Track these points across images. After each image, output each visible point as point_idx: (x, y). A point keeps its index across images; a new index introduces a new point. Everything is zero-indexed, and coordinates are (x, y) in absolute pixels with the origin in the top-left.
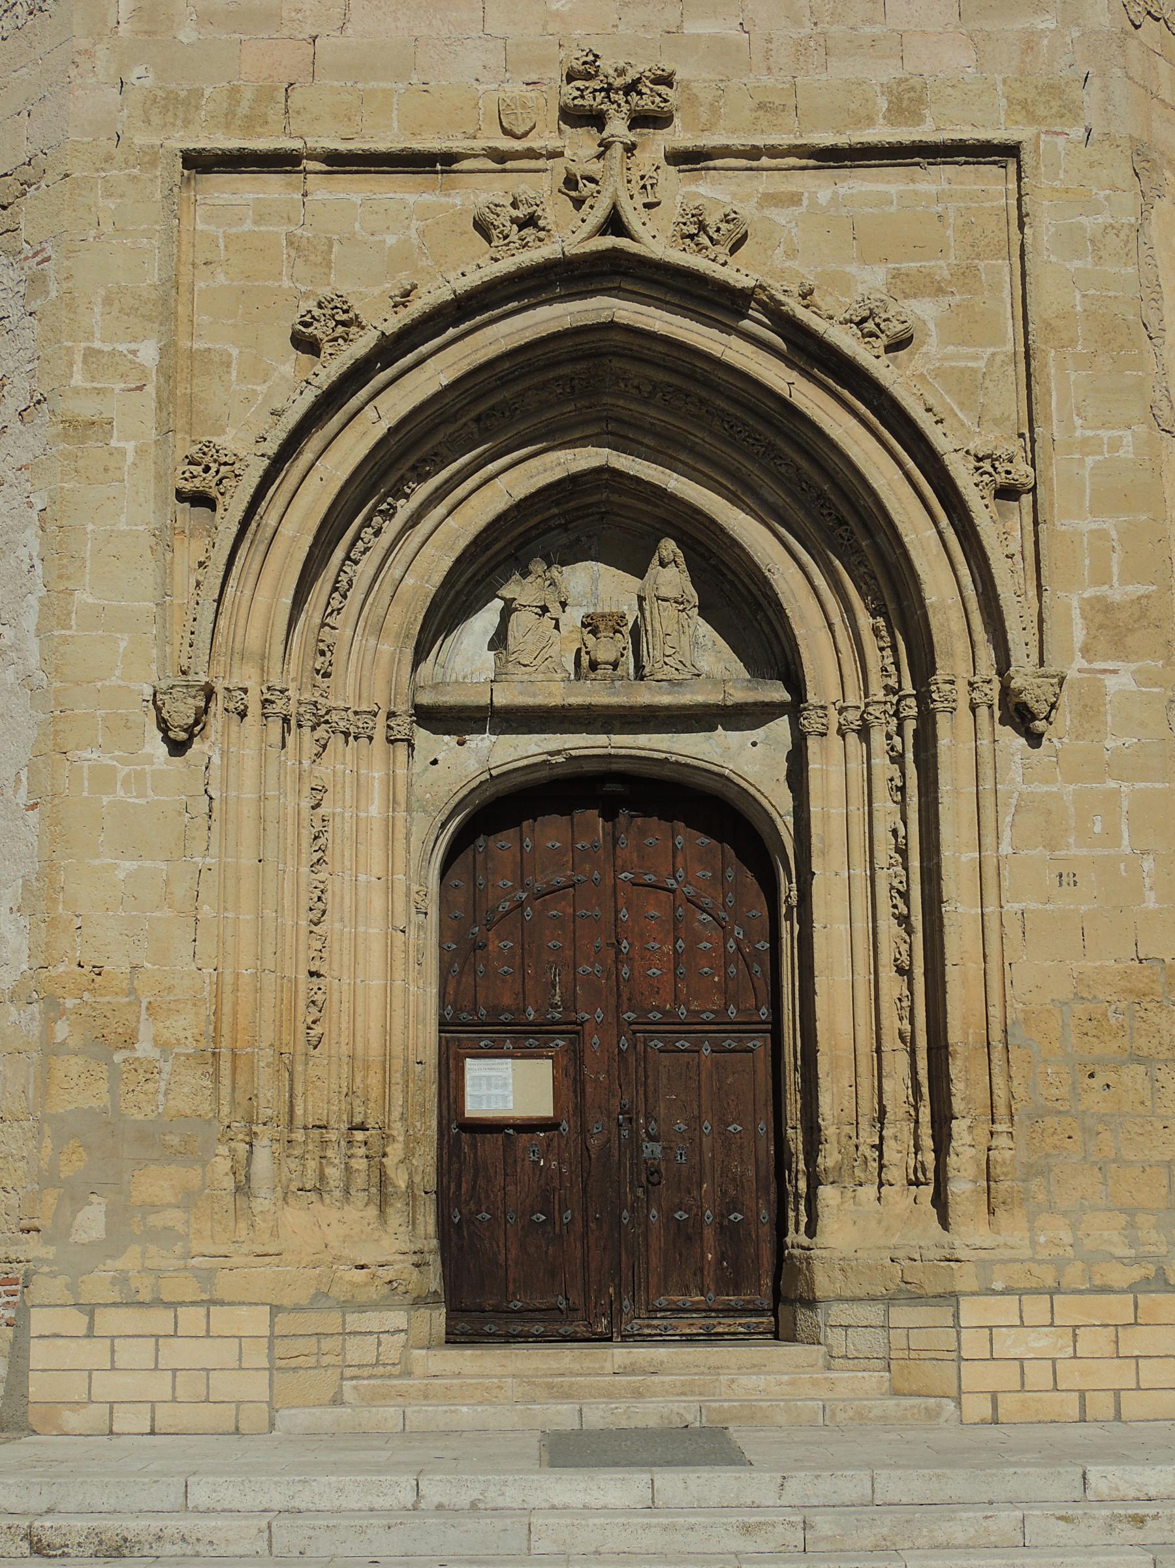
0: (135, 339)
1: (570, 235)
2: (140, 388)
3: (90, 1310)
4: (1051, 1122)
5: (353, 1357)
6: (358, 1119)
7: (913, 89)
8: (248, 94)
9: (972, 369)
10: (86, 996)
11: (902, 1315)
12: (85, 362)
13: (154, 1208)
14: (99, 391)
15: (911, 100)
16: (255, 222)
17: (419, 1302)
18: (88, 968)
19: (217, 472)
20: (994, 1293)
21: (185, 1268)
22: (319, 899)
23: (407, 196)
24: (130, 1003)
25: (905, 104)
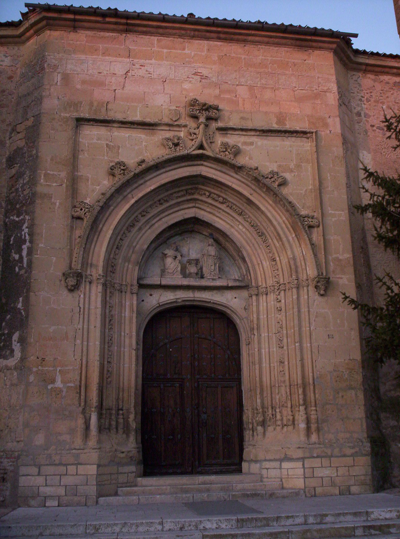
0: (60, 171)
1: (190, 148)
3: (39, 467)
4: (328, 406)
5: (121, 480)
6: (120, 407)
10: (40, 367)
11: (285, 465)
13: (60, 434)
16: (97, 140)
17: (366, 455)
18: (40, 359)
19: (85, 210)
20: (314, 457)
21: (70, 453)
22: (111, 340)
23: (142, 136)
24: (54, 370)
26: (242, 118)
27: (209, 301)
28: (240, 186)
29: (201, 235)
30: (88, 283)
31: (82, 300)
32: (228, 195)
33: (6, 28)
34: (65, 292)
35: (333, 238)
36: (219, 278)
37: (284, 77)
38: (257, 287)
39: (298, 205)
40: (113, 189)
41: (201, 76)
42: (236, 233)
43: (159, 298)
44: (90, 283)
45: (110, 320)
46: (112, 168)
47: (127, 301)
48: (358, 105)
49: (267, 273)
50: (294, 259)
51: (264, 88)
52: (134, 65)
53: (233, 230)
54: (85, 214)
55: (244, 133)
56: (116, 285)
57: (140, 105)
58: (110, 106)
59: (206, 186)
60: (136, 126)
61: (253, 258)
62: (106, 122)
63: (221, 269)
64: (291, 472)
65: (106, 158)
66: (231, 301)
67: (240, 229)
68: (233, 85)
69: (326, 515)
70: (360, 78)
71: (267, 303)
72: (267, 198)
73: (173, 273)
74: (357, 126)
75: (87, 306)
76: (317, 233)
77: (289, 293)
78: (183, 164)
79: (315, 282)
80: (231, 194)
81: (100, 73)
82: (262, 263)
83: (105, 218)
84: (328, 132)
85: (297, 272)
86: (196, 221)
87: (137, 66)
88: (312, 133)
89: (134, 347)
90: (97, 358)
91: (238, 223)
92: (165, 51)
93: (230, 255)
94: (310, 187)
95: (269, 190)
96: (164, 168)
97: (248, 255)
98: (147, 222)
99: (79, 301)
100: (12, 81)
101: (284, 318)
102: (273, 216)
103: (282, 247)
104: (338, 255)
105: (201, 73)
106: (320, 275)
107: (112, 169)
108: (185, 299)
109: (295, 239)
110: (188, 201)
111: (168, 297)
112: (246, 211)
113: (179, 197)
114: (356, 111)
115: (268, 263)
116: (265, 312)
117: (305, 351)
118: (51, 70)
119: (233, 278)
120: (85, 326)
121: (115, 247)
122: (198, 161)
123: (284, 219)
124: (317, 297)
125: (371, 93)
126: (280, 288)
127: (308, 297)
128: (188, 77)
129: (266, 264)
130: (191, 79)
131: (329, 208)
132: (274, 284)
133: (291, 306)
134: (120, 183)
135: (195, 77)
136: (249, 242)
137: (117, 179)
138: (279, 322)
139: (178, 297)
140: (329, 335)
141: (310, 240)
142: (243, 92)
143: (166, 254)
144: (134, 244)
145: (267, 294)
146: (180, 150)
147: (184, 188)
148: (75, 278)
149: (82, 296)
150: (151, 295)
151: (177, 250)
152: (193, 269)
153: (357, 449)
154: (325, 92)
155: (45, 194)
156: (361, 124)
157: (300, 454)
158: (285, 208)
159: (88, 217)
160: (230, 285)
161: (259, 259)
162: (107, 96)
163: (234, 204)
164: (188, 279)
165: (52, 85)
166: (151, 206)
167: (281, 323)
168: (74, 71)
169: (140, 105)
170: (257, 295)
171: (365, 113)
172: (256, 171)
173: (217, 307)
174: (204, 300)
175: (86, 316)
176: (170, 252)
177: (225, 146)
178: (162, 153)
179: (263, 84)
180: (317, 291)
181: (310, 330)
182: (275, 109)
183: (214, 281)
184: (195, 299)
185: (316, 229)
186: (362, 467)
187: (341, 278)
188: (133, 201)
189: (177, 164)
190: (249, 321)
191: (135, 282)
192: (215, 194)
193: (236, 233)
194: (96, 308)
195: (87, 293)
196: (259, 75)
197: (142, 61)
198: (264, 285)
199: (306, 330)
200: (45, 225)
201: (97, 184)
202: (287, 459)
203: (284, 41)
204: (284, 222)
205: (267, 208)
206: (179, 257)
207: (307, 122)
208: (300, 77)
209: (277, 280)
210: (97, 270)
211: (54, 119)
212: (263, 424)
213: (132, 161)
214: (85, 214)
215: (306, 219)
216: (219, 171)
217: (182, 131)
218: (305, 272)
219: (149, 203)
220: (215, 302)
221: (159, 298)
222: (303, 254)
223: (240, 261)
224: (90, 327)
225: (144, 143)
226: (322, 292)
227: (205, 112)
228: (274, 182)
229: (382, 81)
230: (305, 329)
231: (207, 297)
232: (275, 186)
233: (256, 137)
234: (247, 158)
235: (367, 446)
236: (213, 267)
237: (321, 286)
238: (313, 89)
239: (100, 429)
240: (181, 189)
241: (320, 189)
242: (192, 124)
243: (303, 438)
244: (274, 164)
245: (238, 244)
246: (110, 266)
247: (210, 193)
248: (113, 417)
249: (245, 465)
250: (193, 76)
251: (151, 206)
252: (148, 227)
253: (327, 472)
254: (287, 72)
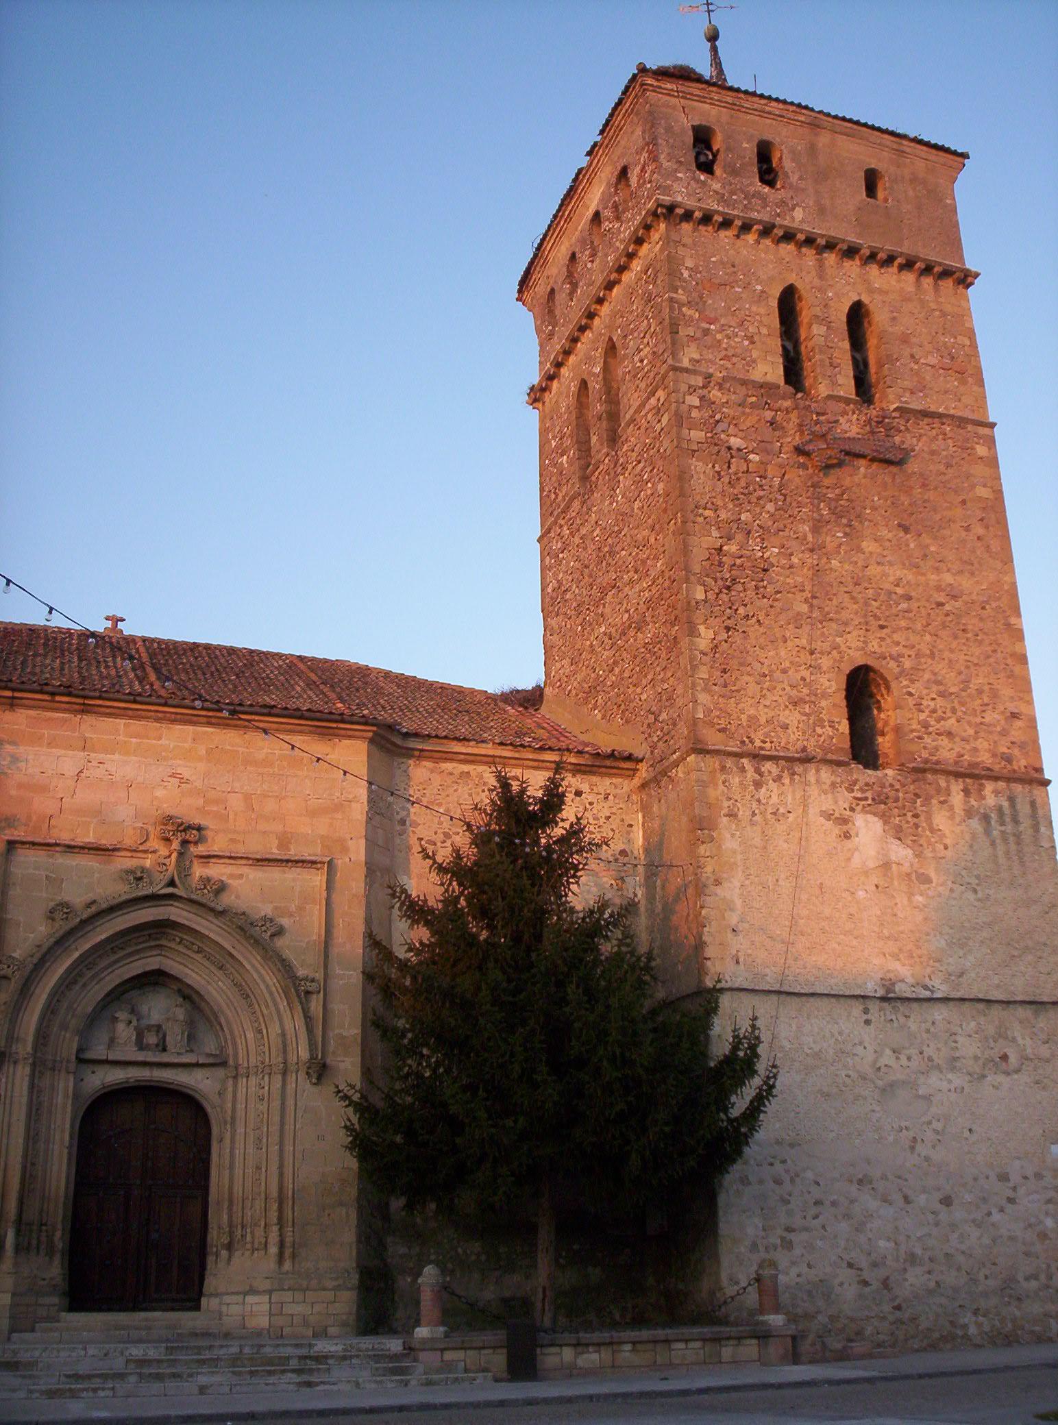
11: (250, 1299)
17: (349, 1289)
26: (232, 840)
28: (219, 935)
35: (337, 1007)
40: (52, 940)
42: (214, 992)
44: (15, 1063)
48: (403, 808)
55: (232, 861)
63: (191, 1038)
64: (255, 1308)
66: (201, 1083)
69: (264, 1346)
71: (248, 1088)
73: (125, 1044)
74: (398, 841)
75: (9, 1093)
87: (94, 763)
89: (67, 1143)
90: (19, 1159)
92: (134, 740)
95: (257, 942)
98: (93, 977)
106: (313, 1057)
110: (151, 947)
111: (117, 1076)
114: (399, 817)
117: (286, 1155)
119: (208, 1050)
124: (308, 1085)
126: (266, 1070)
129: (250, 1035)
134: (61, 932)
137: (57, 925)
142: (236, 802)
151: (133, 1011)
152: (152, 1039)
153: (340, 1282)
157: (267, 1285)
162: (50, 806)
169: (95, 820)
176: (122, 1015)
177: (206, 881)
178: (122, 891)
182: (277, 827)
185: (315, 996)
186: (345, 1303)
188: (76, 955)
191: (74, 1057)
197: (101, 756)
199: (289, 1127)
202: (252, 1291)
203: (299, 728)
206: (135, 1023)
212: (229, 1247)
225: (96, 875)
226: (314, 1080)
235: (355, 1279)
239: (18, 1249)
243: (273, 1265)
246: (42, 1037)
247: (182, 939)
248: (34, 1235)
249: (204, 1301)
253: (298, 1309)
254: (299, 773)
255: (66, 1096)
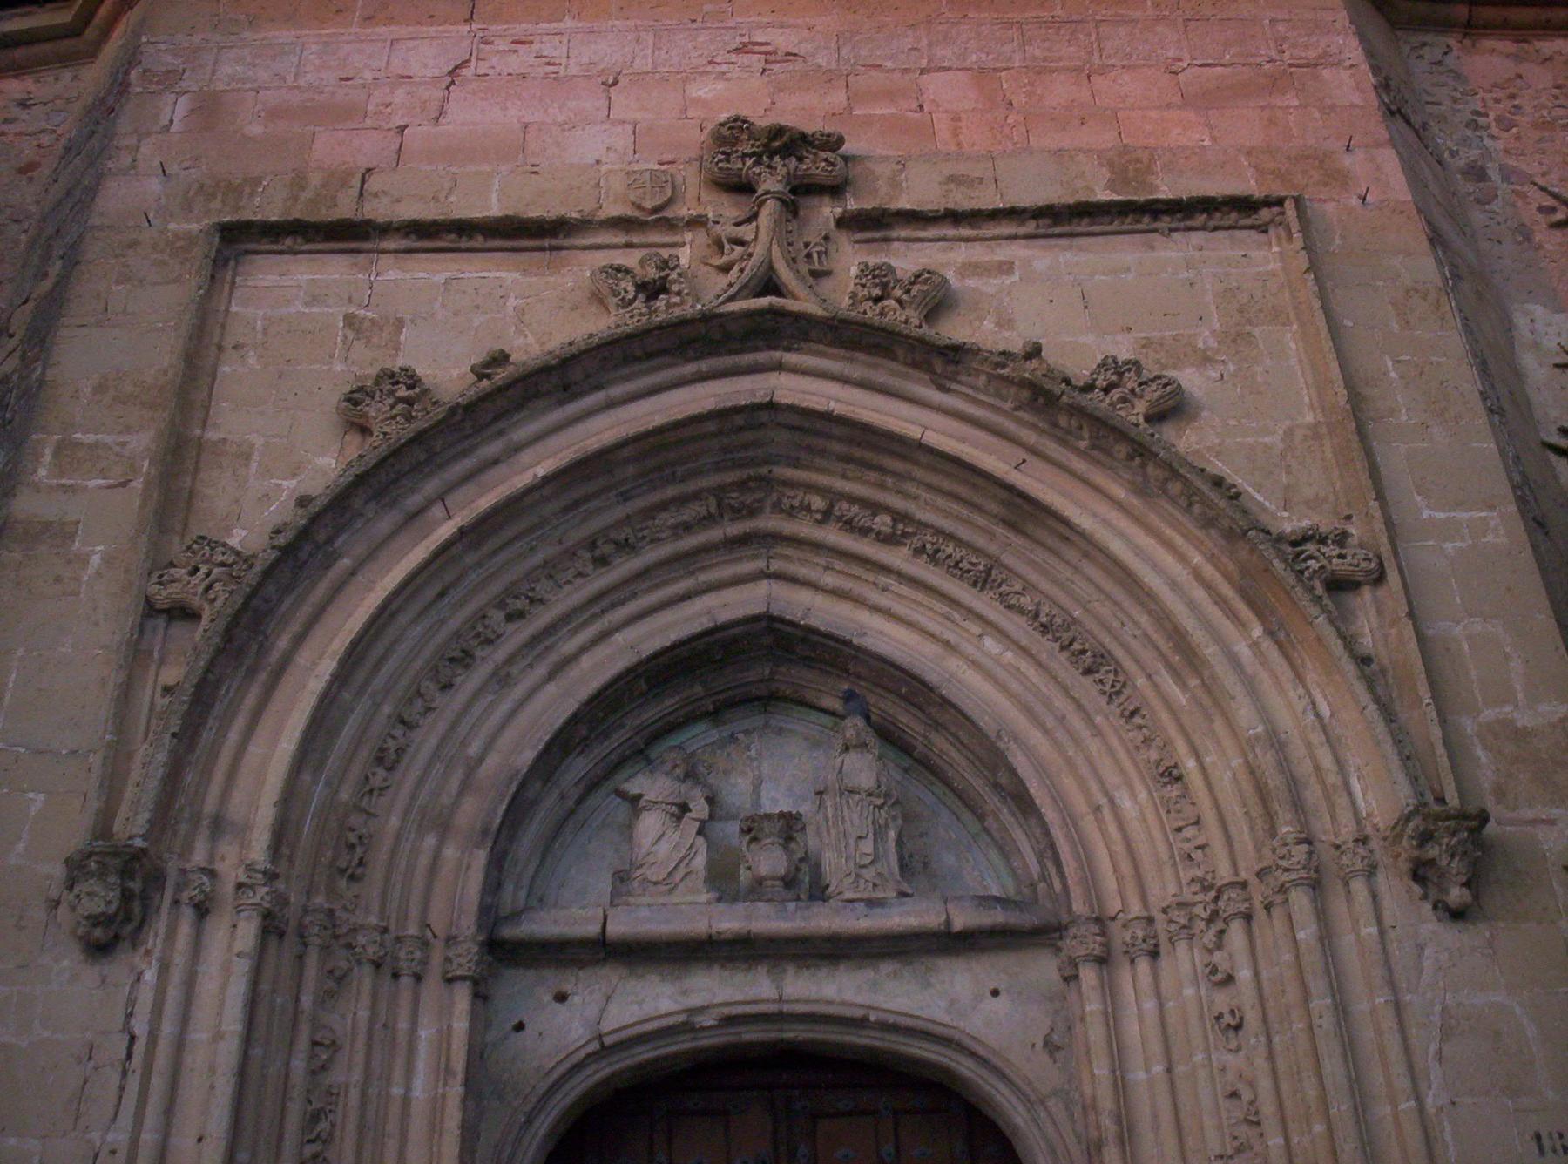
0: (128, 429)
2: (124, 484)
7: (1138, 161)
8: (315, 179)
9: (1266, 445)
12: (56, 454)
14: (65, 489)
15: (1136, 170)
16: (307, 304)
19: (208, 575)
23: (504, 275)
25: (1131, 174)
27: (859, 1013)
29: (814, 716)
30: (188, 914)
31: (146, 997)
32: (916, 498)
33: (27, 9)
34: (69, 959)
35: (1459, 630)
36: (903, 894)
37: (1122, 31)
38: (1098, 920)
39: (1259, 497)
41: (766, 53)
43: (603, 1010)
44: (202, 910)
45: (315, 1117)
46: (353, 399)
47: (424, 1019)
48: (1465, 142)
49: (1142, 848)
50: (1275, 740)
51: (1041, 70)
52: (487, 43)
53: (954, 664)
54: (209, 587)
55: (966, 232)
56: (361, 939)
57: (503, 168)
58: (374, 183)
59: (807, 468)
60: (479, 241)
61: (1068, 782)
62: (348, 234)
65: (338, 367)
66: (970, 1009)
67: (988, 654)
68: (905, 71)
70: (1455, 53)
71: (1158, 1003)
72: (1099, 478)
73: (669, 884)
74: (1477, 217)
75: (168, 1028)
76: (1379, 612)
77: (1270, 930)
78: (689, 369)
79: (1407, 846)
80: (929, 487)
81: (347, 79)
82: (1112, 801)
83: (306, 610)
84: (1354, 201)
85: (1298, 805)
86: (777, 638)
87: (502, 45)
88: (1280, 202)
91: (976, 629)
93: (959, 794)
94: (1309, 418)
96: (599, 387)
97: (1041, 768)
99: (131, 1001)
100: (31, 179)
101: (1261, 1063)
102: (1138, 551)
103: (1207, 702)
104: (1508, 709)
105: (767, 44)
107: (356, 403)
108: (739, 1010)
109: (1267, 644)
111: (647, 1002)
112: (1007, 559)
113: (687, 528)
115: (1143, 795)
116: (1156, 1047)
118: (153, 88)
120: (148, 1137)
121: (364, 754)
122: (756, 349)
123: (1197, 559)
124: (1430, 926)
125: (1512, 97)
126: (1219, 907)
127: (1382, 933)
128: (710, 62)
130: (724, 68)
131: (1419, 498)
132: (1187, 896)
133: (1293, 994)
135: (743, 59)
136: (1038, 708)
138: (1234, 1095)
139: (696, 1000)
140: (1538, 1137)
141: (1349, 642)
143: (640, 796)
144: (474, 749)
145: (1154, 954)
146: (668, 306)
147: (704, 483)
148: (113, 879)
149: (150, 976)
150: (561, 998)
152: (769, 861)
154: (1316, 65)
155: (48, 525)
156: (1495, 206)
158: (1197, 509)
159: (218, 603)
160: (959, 924)
161: (1093, 786)
162: (366, 148)
163: (951, 537)
164: (741, 907)
165: (149, 134)
166: (550, 569)
167: (1247, 1096)
168: (243, 81)
170: (1103, 961)
171: (1501, 168)
172: (1035, 363)
173: (903, 1049)
174: (831, 1010)
175: (158, 1083)
179: (1035, 58)
180: (1425, 897)
181: (1421, 1109)
182: (1106, 139)
183: (878, 910)
184: (786, 1008)
185: (1366, 592)
187: (1551, 822)
188: (446, 531)
189: (659, 368)
190: (1077, 1110)
191: (468, 925)
192: (852, 499)
193: (972, 677)
194: (218, 1036)
195: (180, 959)
196: (1014, 33)
198: (1136, 909)
200: (20, 652)
201: (279, 456)
204: (1197, 574)
205: (1106, 523)
207: (1250, 172)
208: (1192, 25)
209: (1200, 874)
210: (244, 845)
211: (133, 244)
213: (455, 373)
214: (209, 587)
215: (1310, 548)
216: (862, 384)
217: (683, 245)
218: (1342, 801)
219: (538, 558)
220: (891, 1019)
221: (603, 1010)
222: (1318, 715)
223: (1006, 815)
224: (173, 1140)
226: (1456, 895)
227: (783, 166)
228: (1124, 400)
229: (1550, 59)
230: (1388, 1109)
231: (849, 996)
232: (1133, 419)
233: (1023, 242)
234: (988, 325)
236: (867, 847)
237: (1444, 862)
238: (1259, 60)
240: (690, 487)
241: (1358, 415)
242: (723, 210)
244: (1119, 337)
245: (986, 723)
250: (733, 58)
251: (550, 569)
252: (541, 670)
254: (1138, 14)
255: (443, 1071)
